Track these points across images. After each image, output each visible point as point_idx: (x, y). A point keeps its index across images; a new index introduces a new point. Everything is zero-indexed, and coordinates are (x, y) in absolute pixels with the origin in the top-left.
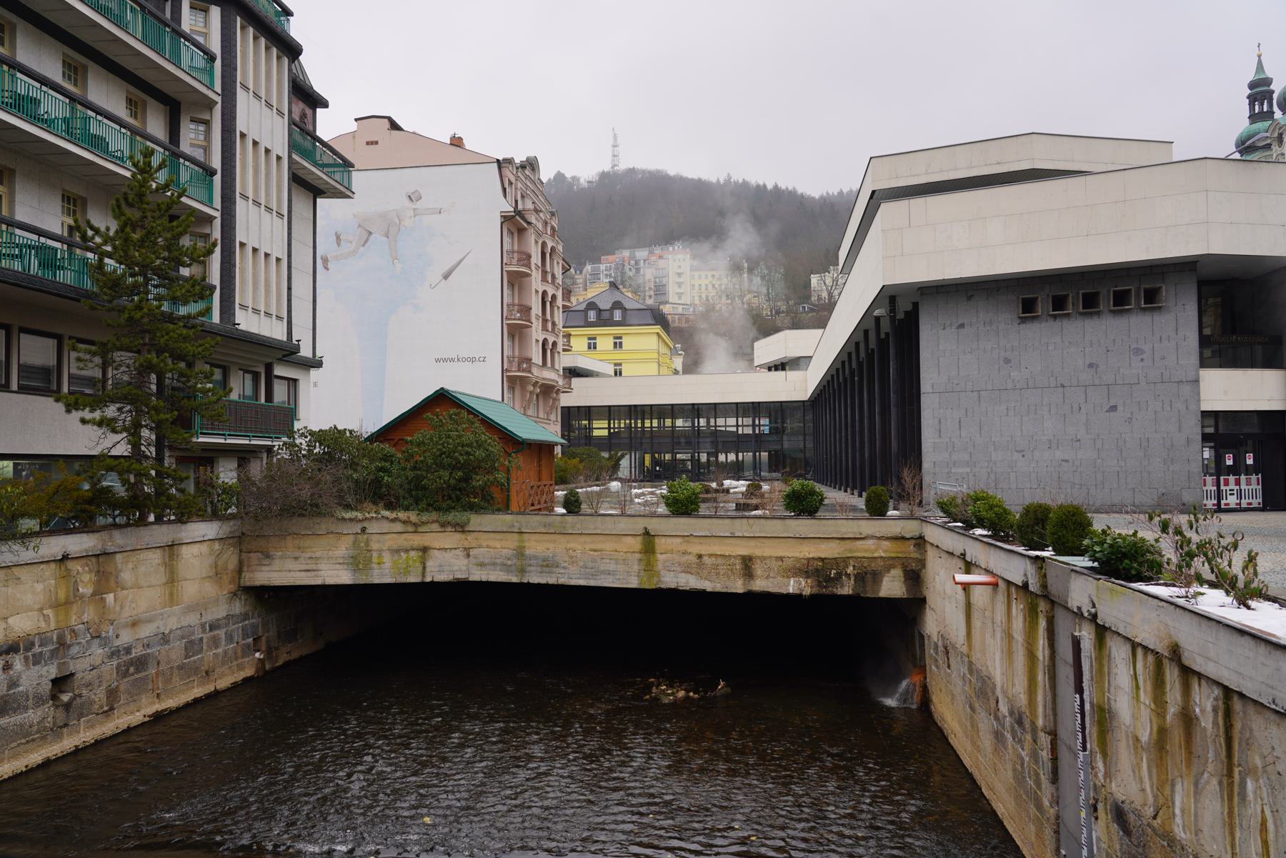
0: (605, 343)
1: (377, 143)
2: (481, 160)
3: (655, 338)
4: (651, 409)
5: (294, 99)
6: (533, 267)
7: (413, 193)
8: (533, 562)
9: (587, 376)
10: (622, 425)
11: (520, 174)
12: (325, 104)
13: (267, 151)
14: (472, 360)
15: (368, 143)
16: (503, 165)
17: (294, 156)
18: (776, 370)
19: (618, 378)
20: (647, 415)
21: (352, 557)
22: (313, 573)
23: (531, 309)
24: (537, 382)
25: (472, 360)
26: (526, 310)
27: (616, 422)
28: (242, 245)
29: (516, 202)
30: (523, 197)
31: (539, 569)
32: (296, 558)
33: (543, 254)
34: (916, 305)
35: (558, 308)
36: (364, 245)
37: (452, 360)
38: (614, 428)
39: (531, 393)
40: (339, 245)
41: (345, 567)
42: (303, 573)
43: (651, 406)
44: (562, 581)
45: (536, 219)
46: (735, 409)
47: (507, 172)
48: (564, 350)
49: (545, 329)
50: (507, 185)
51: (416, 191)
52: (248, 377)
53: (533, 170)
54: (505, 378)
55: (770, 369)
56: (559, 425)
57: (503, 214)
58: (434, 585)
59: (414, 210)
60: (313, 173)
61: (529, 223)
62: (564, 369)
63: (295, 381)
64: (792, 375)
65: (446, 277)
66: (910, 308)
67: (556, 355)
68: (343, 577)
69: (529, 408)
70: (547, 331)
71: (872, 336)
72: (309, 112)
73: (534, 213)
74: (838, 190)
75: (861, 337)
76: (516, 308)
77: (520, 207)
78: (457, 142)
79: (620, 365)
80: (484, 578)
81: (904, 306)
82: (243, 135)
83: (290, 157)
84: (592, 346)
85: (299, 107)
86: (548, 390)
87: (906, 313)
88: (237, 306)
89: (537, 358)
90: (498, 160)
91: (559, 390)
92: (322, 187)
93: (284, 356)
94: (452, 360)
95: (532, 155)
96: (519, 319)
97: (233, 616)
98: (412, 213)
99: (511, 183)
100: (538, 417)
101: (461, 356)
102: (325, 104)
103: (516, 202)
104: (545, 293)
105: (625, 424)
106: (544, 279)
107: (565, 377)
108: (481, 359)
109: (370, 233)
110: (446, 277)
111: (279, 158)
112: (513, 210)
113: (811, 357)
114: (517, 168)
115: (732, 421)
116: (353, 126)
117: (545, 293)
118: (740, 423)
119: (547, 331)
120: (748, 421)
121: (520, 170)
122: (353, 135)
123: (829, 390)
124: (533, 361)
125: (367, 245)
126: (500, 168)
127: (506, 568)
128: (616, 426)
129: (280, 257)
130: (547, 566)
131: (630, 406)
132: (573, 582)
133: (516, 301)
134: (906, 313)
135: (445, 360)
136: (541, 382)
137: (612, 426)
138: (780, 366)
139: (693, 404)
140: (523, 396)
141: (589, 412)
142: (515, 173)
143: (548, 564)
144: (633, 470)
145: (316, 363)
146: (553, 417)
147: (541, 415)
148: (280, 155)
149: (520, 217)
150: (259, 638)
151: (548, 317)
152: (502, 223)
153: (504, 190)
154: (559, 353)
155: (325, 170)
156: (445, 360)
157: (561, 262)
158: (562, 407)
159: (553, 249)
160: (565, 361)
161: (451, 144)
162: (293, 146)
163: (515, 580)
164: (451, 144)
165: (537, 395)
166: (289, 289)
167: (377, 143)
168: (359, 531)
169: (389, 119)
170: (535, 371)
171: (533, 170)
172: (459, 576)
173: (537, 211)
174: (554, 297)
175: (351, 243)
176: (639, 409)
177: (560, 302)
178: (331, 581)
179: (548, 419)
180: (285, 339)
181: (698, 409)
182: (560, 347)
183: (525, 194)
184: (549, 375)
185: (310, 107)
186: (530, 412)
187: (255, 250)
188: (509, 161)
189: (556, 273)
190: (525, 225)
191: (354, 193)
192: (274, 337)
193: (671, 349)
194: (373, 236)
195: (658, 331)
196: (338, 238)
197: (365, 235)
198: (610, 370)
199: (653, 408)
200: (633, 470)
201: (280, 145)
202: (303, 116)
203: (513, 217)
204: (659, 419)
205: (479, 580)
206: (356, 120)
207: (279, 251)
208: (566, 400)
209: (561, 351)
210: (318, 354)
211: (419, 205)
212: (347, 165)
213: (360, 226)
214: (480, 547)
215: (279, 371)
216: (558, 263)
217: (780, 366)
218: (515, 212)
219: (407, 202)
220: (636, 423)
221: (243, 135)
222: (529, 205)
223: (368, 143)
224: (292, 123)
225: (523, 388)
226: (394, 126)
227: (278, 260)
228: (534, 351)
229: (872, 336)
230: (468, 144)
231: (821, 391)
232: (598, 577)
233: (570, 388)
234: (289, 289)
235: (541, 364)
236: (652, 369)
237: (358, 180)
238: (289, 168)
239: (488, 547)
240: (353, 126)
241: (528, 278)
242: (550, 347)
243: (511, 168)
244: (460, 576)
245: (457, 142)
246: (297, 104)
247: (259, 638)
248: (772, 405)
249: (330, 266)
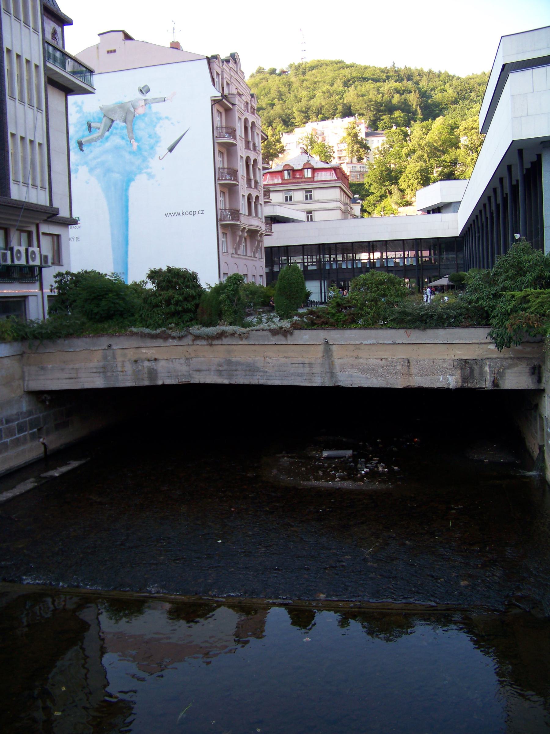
0: (299, 196)
1: (115, 51)
2: (196, 59)
3: (338, 191)
4: (336, 246)
5: (45, 18)
6: (238, 138)
7: (143, 88)
8: (239, 368)
9: (285, 222)
10: (314, 260)
11: (225, 67)
12: (70, 23)
13: (28, 62)
14: (194, 213)
15: (108, 52)
16: (212, 60)
17: (48, 64)
18: (433, 213)
19: (310, 223)
20: (333, 252)
21: (103, 367)
22: (77, 380)
23: (237, 171)
24: (244, 228)
25: (194, 213)
26: (233, 173)
27: (309, 257)
28: (13, 135)
29: (223, 88)
30: (228, 84)
31: (244, 373)
32: (62, 370)
33: (246, 128)
34: (539, 157)
35: (259, 169)
36: (108, 130)
37: (178, 214)
38: (308, 262)
39: (241, 237)
40: (90, 131)
41: (98, 375)
42: (68, 381)
43: (336, 244)
44: (262, 382)
45: (239, 100)
46: (402, 245)
47: (217, 68)
48: (265, 202)
49: (249, 186)
50: (215, 77)
51: (146, 86)
52: (24, 236)
53: (236, 63)
54: (219, 227)
55: (429, 212)
56: (264, 261)
57: (213, 99)
58: (164, 387)
59: (145, 100)
60: (63, 76)
61: (233, 105)
62: (266, 218)
63: (58, 236)
64: (445, 217)
65: (171, 150)
66: (535, 159)
67: (259, 206)
68: (99, 383)
69: (239, 249)
70: (251, 187)
71: (506, 183)
72: (59, 30)
73: (237, 96)
74: (482, 71)
75: (497, 184)
76: (226, 171)
77: (226, 92)
78: (175, 46)
79: (311, 213)
80: (202, 381)
81: (529, 159)
82: (9, 51)
83: (45, 65)
84: (289, 199)
85: (50, 25)
86: (253, 234)
87: (532, 163)
88: (11, 182)
89: (243, 207)
90: (207, 58)
91: (262, 234)
92: (70, 86)
93: (49, 218)
94: (178, 214)
95: (233, 52)
96: (229, 180)
97: (21, 413)
98: (143, 103)
99: (218, 74)
100: (246, 256)
101: (184, 211)
102: (70, 23)
103: (223, 88)
104: (248, 159)
105: (316, 258)
106: (247, 147)
107: (267, 223)
108: (201, 212)
109: (113, 121)
110: (171, 150)
111: (37, 67)
112: (220, 95)
113: (460, 202)
114: (223, 62)
115: (399, 254)
116: (97, 40)
117: (248, 159)
118: (406, 256)
119: (251, 187)
120: (412, 254)
121: (225, 63)
122: (98, 47)
123: (486, 214)
124: (241, 212)
125: (110, 130)
126: (209, 63)
127: (219, 372)
128: (309, 261)
129: (41, 142)
130: (250, 371)
131: (319, 245)
132: (270, 383)
133: (226, 166)
134: (532, 163)
135: (173, 215)
136: (247, 228)
137: (306, 261)
138: (437, 209)
139: (369, 242)
140: (234, 240)
141: (287, 250)
142: (221, 66)
143: (252, 369)
144: (323, 294)
145: (71, 222)
146: (257, 255)
147: (249, 254)
148: (38, 64)
149: (226, 100)
150: (41, 428)
151: (252, 177)
152: (212, 105)
153: (213, 80)
154: (261, 204)
155: (75, 76)
156: (173, 215)
157: (260, 133)
158: (266, 248)
159: (253, 123)
160: (268, 211)
161: (171, 47)
162: (47, 56)
163: (226, 382)
164: (171, 47)
165: (245, 239)
166: (49, 166)
167: (115, 51)
168: (106, 348)
169: (123, 32)
170: (242, 219)
171: (236, 63)
172: (183, 380)
173: (240, 95)
174: (255, 161)
175: (99, 129)
176: (326, 246)
177: (260, 165)
178: (88, 385)
179: (254, 257)
180: (48, 204)
181: (373, 246)
182: (262, 200)
183: (229, 83)
184: (257, 223)
185: (59, 25)
186: (239, 252)
187: (22, 138)
188: (215, 57)
189: (257, 143)
190: (230, 106)
191: (95, 89)
192: (30, 202)
193: (351, 198)
194: (115, 123)
195: (340, 185)
196: (89, 126)
197: (109, 122)
198: (302, 216)
199: (338, 245)
200: (323, 294)
201: (37, 58)
202: (54, 33)
203: (221, 100)
204: (343, 254)
205: (198, 382)
206: (99, 35)
207: (40, 138)
208: (268, 242)
209: (262, 203)
210: (74, 216)
211: (149, 96)
212: (90, 71)
213: (105, 116)
214: (197, 357)
215: (44, 228)
216: (258, 134)
217: (437, 209)
218: (222, 96)
219: (139, 95)
220: (324, 258)
221: (9, 51)
222: (234, 91)
223: (108, 52)
224: (45, 42)
225: (234, 234)
226: (127, 37)
227: (40, 145)
228: (241, 204)
229: (506, 183)
230: (185, 46)
231: (469, 228)
232: (289, 378)
233: (271, 232)
234: (49, 166)
235: (247, 214)
236: (337, 214)
237: (97, 81)
238: (45, 74)
239: (204, 356)
240: (97, 40)
241: (235, 147)
242: (254, 201)
243: (217, 63)
244: (184, 380)
245: (175, 46)
246: (49, 24)
247: (41, 428)
248: (431, 240)
249: (84, 148)
